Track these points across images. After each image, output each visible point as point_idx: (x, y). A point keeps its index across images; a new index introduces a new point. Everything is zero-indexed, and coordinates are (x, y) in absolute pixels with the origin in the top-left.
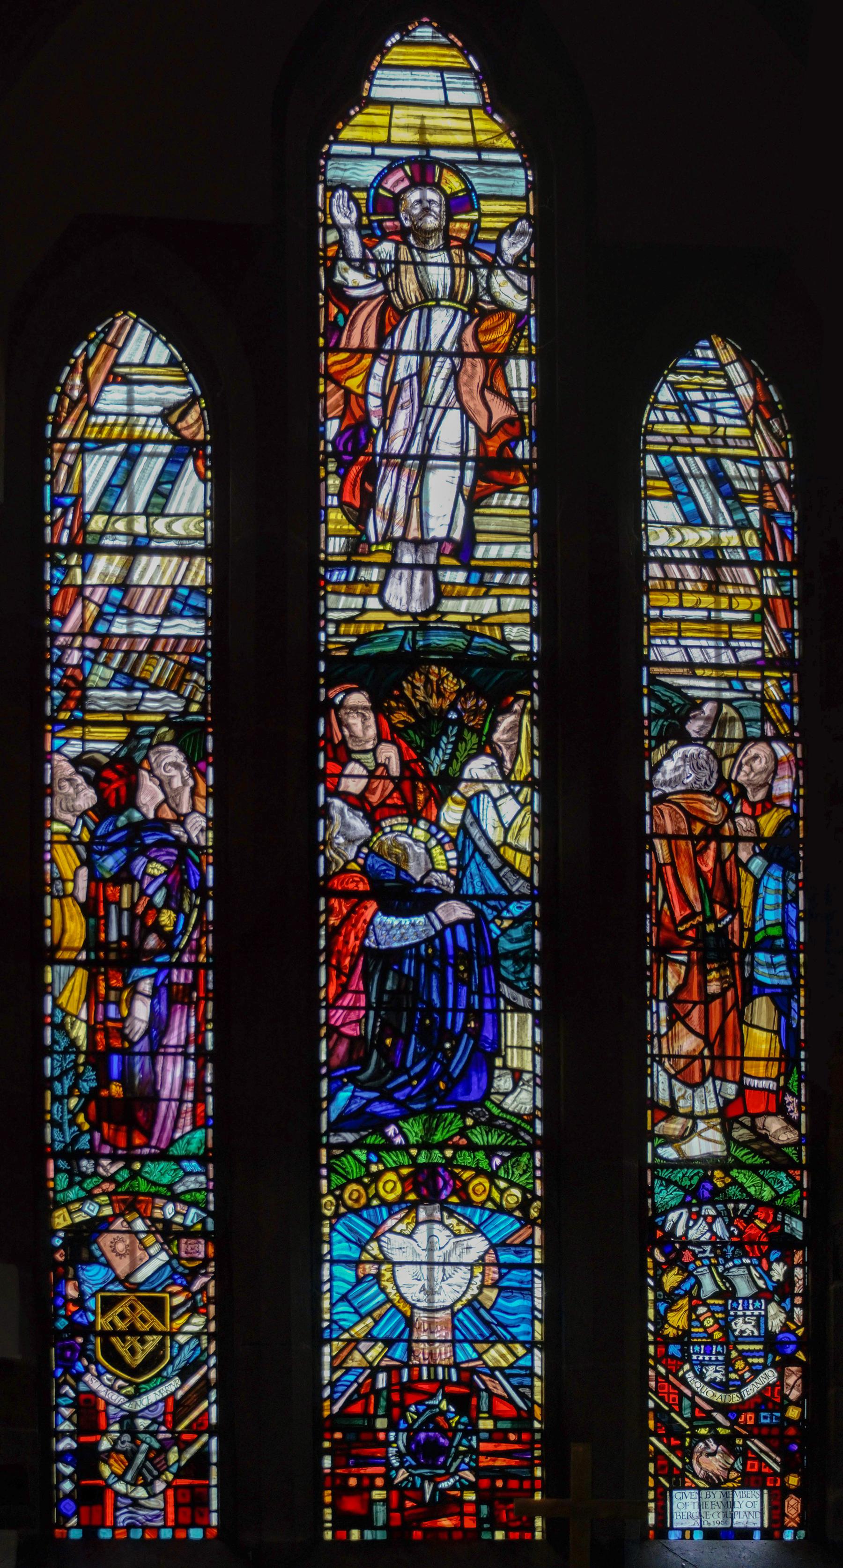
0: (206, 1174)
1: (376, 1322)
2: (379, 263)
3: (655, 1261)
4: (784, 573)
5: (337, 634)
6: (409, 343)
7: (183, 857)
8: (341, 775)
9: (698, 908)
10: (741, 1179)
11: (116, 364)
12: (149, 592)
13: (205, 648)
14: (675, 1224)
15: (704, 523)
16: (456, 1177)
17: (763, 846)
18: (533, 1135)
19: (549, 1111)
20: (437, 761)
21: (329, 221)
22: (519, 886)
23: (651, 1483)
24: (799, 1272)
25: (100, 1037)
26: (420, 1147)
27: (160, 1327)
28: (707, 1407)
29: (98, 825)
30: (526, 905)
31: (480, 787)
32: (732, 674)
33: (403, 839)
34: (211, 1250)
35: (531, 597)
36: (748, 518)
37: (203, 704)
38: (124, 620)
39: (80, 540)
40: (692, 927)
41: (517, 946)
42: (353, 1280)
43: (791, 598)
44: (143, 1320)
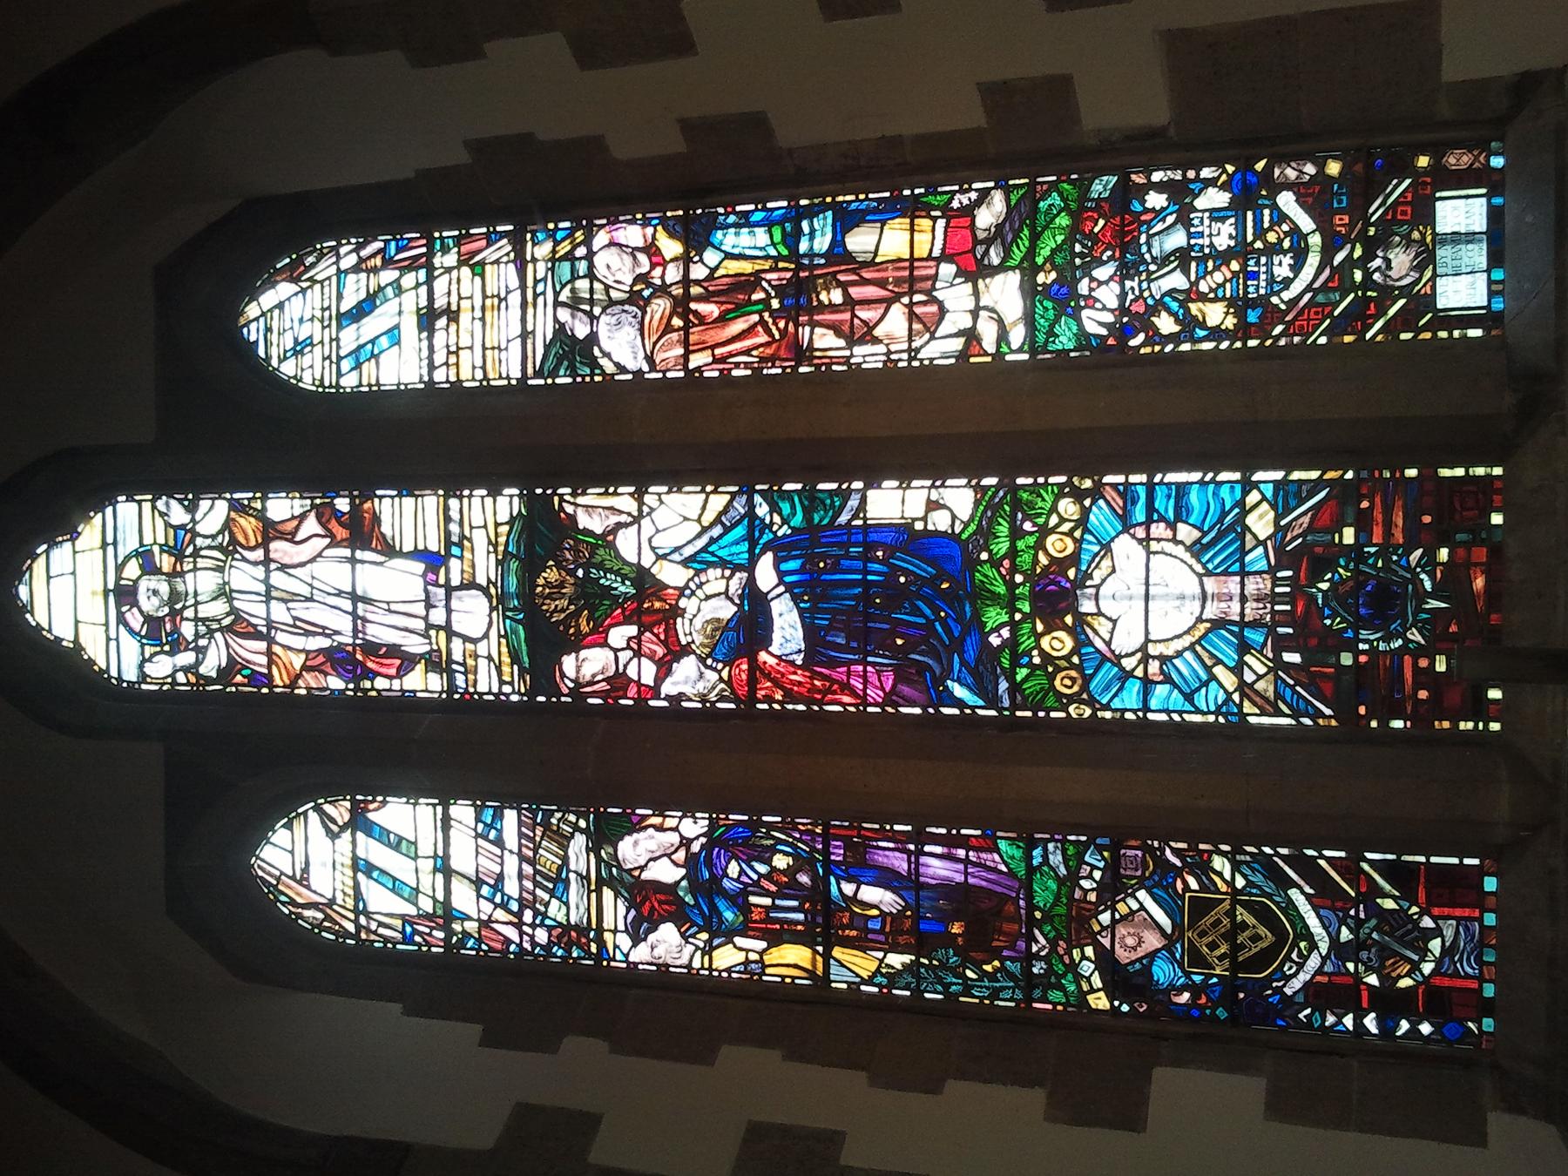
1: (1219, 662)
2: (197, 636)
3: (1143, 345)
4: (438, 246)
8: (638, 683)
9: (756, 318)
10: (1046, 252)
11: (293, 878)
14: (1100, 324)
18: (998, 487)
19: (971, 470)
22: (740, 506)
23: (1428, 335)
24: (1157, 176)
26: (1013, 610)
27: (1226, 905)
28: (1327, 272)
30: (758, 499)
31: (645, 546)
35: (470, 496)
37: (579, 815)
40: (775, 324)
42: (1167, 687)
44: (1219, 921)
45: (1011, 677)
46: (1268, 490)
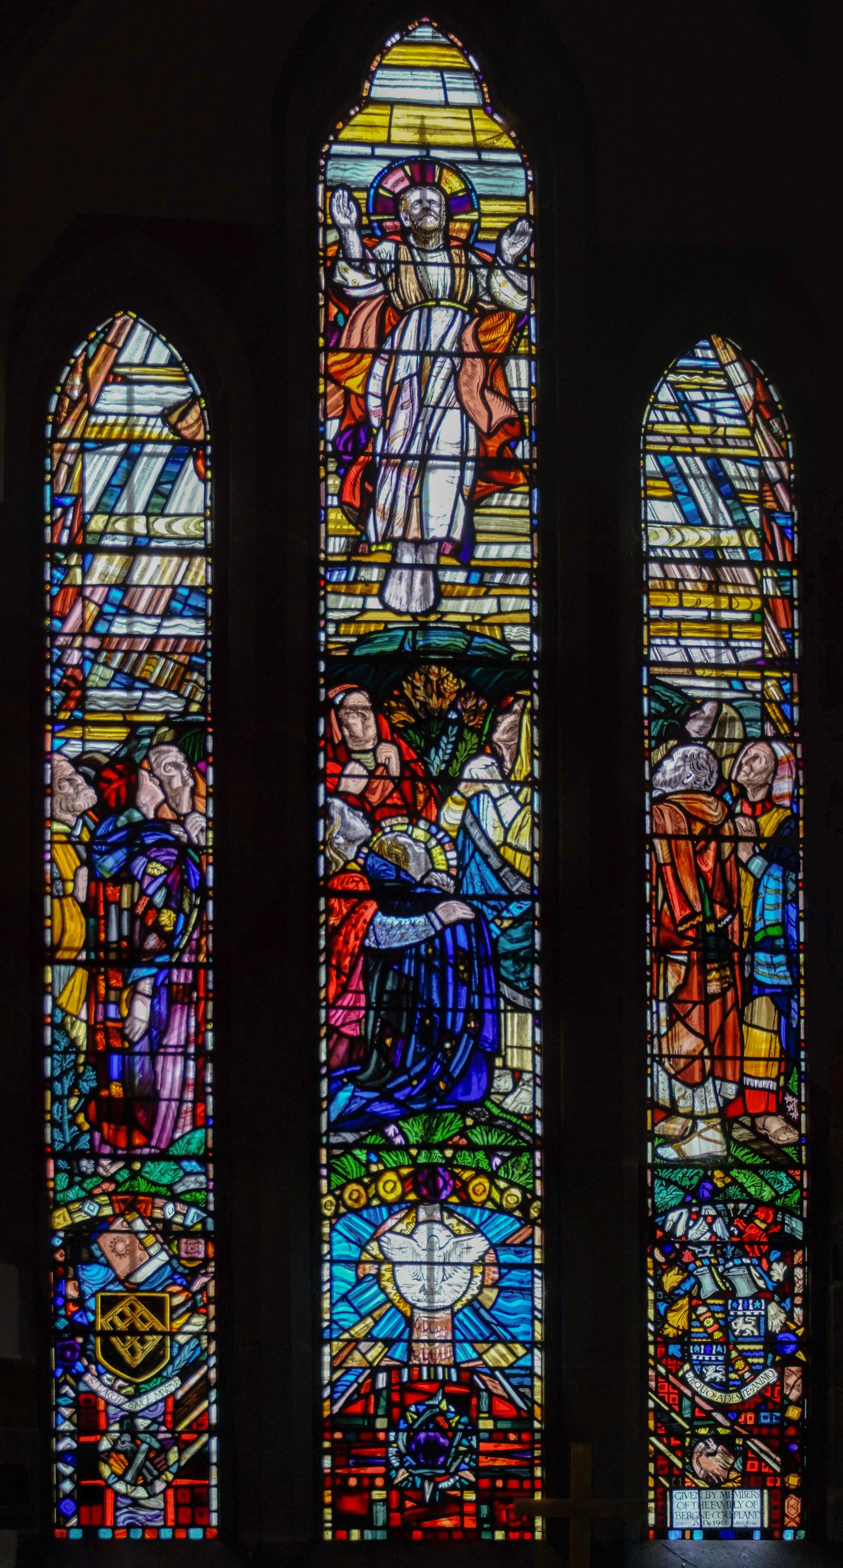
0: (206, 1174)
1: (376, 1322)
2: (379, 263)
3: (655, 1261)
4: (784, 573)
5: (337, 634)
6: (409, 343)
7: (183, 857)
8: (341, 775)
9: (698, 908)
10: (741, 1179)
11: (116, 364)
12: (149, 592)
13: (205, 648)
14: (675, 1224)
15: (704, 523)
16: (456, 1177)
17: (763, 846)
18: (534, 1135)
19: (549, 1111)
20: (437, 761)
21: (329, 221)
22: (519, 886)
23: (651, 1483)
24: (799, 1272)
25: (100, 1037)
26: (420, 1147)
27: (160, 1327)
28: (707, 1407)
29: (98, 825)
30: (526, 905)
31: (480, 787)
32: (732, 674)
33: (403, 839)
34: (211, 1250)
35: (531, 597)
36: (748, 518)
37: (203, 704)
38: (124, 620)
39: (80, 540)
40: (692, 927)
41: (517, 946)
42: (353, 1280)
43: (791, 598)
44: (143, 1320)
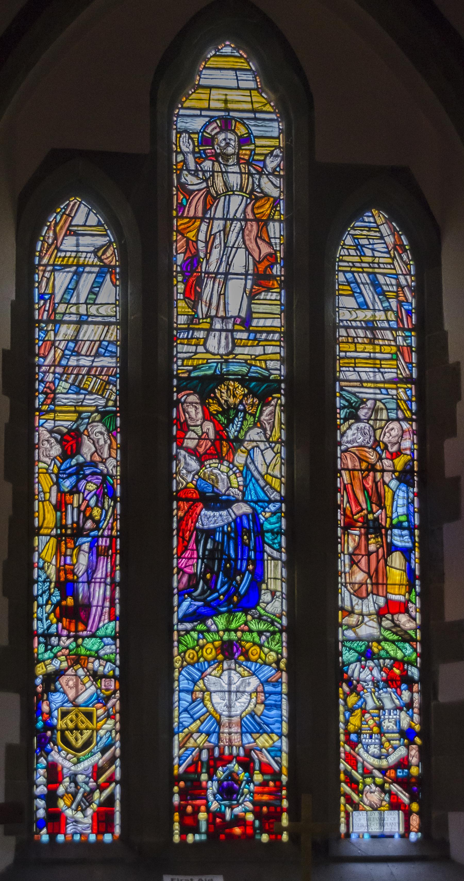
0: (115, 644)
1: (202, 723)
2: (204, 172)
3: (343, 690)
5: (183, 365)
6: (219, 214)
7: (104, 480)
9: (364, 506)
11: (70, 225)
12: (88, 343)
13: (116, 373)
14: (353, 671)
15: (368, 308)
16: (242, 647)
17: (397, 474)
18: (281, 625)
20: (233, 430)
21: (179, 150)
22: (274, 496)
25: (62, 573)
26: (224, 631)
27: (90, 726)
29: (62, 464)
30: (278, 505)
31: (255, 444)
32: (382, 385)
33: (215, 471)
34: (117, 685)
35: (280, 346)
36: (390, 306)
37: (115, 401)
38: (75, 358)
39: (52, 318)
40: (361, 516)
42: (190, 700)
43: (411, 347)
44: (83, 722)
45: (194, 629)
46: (278, 744)
